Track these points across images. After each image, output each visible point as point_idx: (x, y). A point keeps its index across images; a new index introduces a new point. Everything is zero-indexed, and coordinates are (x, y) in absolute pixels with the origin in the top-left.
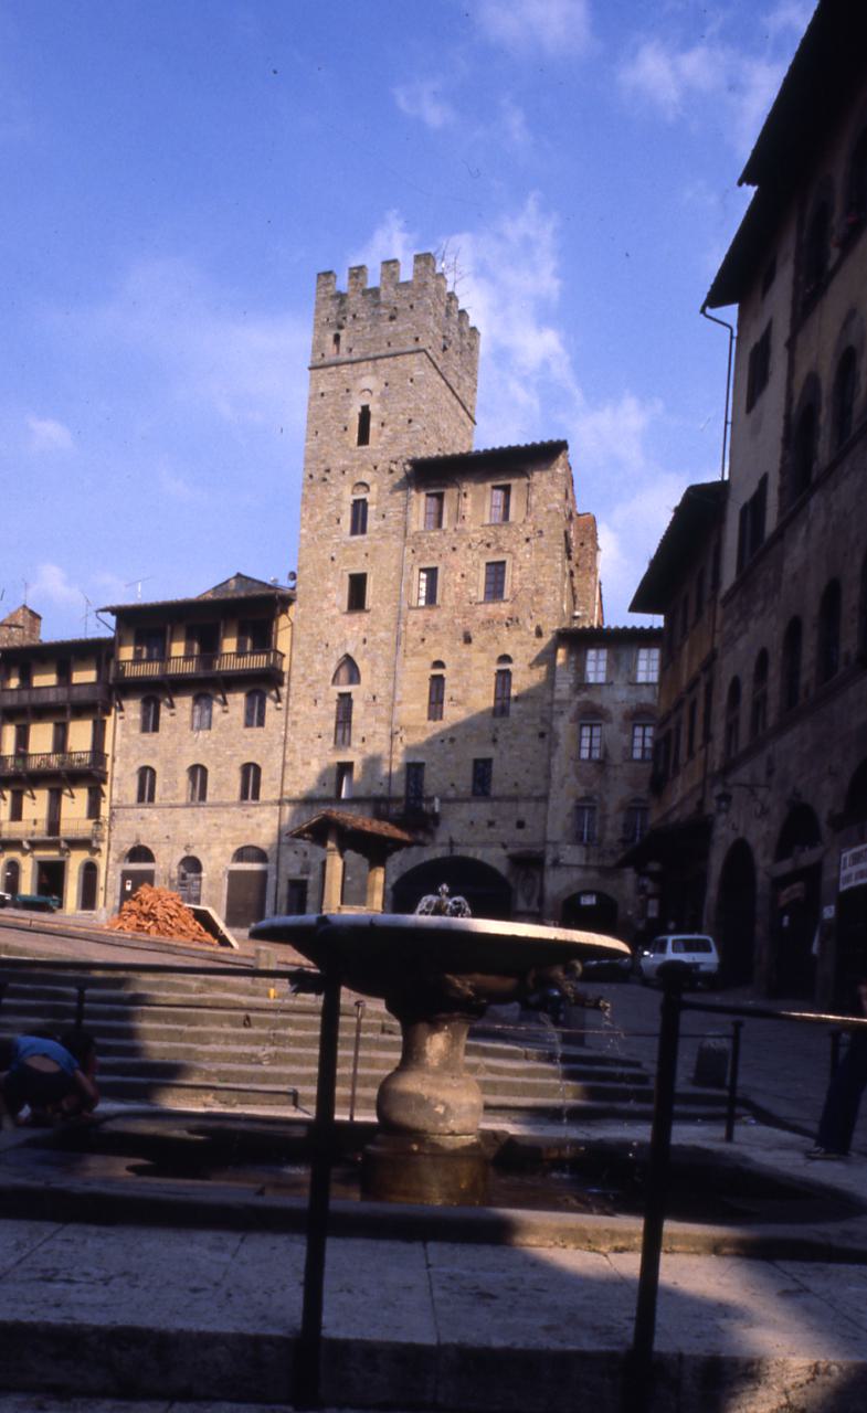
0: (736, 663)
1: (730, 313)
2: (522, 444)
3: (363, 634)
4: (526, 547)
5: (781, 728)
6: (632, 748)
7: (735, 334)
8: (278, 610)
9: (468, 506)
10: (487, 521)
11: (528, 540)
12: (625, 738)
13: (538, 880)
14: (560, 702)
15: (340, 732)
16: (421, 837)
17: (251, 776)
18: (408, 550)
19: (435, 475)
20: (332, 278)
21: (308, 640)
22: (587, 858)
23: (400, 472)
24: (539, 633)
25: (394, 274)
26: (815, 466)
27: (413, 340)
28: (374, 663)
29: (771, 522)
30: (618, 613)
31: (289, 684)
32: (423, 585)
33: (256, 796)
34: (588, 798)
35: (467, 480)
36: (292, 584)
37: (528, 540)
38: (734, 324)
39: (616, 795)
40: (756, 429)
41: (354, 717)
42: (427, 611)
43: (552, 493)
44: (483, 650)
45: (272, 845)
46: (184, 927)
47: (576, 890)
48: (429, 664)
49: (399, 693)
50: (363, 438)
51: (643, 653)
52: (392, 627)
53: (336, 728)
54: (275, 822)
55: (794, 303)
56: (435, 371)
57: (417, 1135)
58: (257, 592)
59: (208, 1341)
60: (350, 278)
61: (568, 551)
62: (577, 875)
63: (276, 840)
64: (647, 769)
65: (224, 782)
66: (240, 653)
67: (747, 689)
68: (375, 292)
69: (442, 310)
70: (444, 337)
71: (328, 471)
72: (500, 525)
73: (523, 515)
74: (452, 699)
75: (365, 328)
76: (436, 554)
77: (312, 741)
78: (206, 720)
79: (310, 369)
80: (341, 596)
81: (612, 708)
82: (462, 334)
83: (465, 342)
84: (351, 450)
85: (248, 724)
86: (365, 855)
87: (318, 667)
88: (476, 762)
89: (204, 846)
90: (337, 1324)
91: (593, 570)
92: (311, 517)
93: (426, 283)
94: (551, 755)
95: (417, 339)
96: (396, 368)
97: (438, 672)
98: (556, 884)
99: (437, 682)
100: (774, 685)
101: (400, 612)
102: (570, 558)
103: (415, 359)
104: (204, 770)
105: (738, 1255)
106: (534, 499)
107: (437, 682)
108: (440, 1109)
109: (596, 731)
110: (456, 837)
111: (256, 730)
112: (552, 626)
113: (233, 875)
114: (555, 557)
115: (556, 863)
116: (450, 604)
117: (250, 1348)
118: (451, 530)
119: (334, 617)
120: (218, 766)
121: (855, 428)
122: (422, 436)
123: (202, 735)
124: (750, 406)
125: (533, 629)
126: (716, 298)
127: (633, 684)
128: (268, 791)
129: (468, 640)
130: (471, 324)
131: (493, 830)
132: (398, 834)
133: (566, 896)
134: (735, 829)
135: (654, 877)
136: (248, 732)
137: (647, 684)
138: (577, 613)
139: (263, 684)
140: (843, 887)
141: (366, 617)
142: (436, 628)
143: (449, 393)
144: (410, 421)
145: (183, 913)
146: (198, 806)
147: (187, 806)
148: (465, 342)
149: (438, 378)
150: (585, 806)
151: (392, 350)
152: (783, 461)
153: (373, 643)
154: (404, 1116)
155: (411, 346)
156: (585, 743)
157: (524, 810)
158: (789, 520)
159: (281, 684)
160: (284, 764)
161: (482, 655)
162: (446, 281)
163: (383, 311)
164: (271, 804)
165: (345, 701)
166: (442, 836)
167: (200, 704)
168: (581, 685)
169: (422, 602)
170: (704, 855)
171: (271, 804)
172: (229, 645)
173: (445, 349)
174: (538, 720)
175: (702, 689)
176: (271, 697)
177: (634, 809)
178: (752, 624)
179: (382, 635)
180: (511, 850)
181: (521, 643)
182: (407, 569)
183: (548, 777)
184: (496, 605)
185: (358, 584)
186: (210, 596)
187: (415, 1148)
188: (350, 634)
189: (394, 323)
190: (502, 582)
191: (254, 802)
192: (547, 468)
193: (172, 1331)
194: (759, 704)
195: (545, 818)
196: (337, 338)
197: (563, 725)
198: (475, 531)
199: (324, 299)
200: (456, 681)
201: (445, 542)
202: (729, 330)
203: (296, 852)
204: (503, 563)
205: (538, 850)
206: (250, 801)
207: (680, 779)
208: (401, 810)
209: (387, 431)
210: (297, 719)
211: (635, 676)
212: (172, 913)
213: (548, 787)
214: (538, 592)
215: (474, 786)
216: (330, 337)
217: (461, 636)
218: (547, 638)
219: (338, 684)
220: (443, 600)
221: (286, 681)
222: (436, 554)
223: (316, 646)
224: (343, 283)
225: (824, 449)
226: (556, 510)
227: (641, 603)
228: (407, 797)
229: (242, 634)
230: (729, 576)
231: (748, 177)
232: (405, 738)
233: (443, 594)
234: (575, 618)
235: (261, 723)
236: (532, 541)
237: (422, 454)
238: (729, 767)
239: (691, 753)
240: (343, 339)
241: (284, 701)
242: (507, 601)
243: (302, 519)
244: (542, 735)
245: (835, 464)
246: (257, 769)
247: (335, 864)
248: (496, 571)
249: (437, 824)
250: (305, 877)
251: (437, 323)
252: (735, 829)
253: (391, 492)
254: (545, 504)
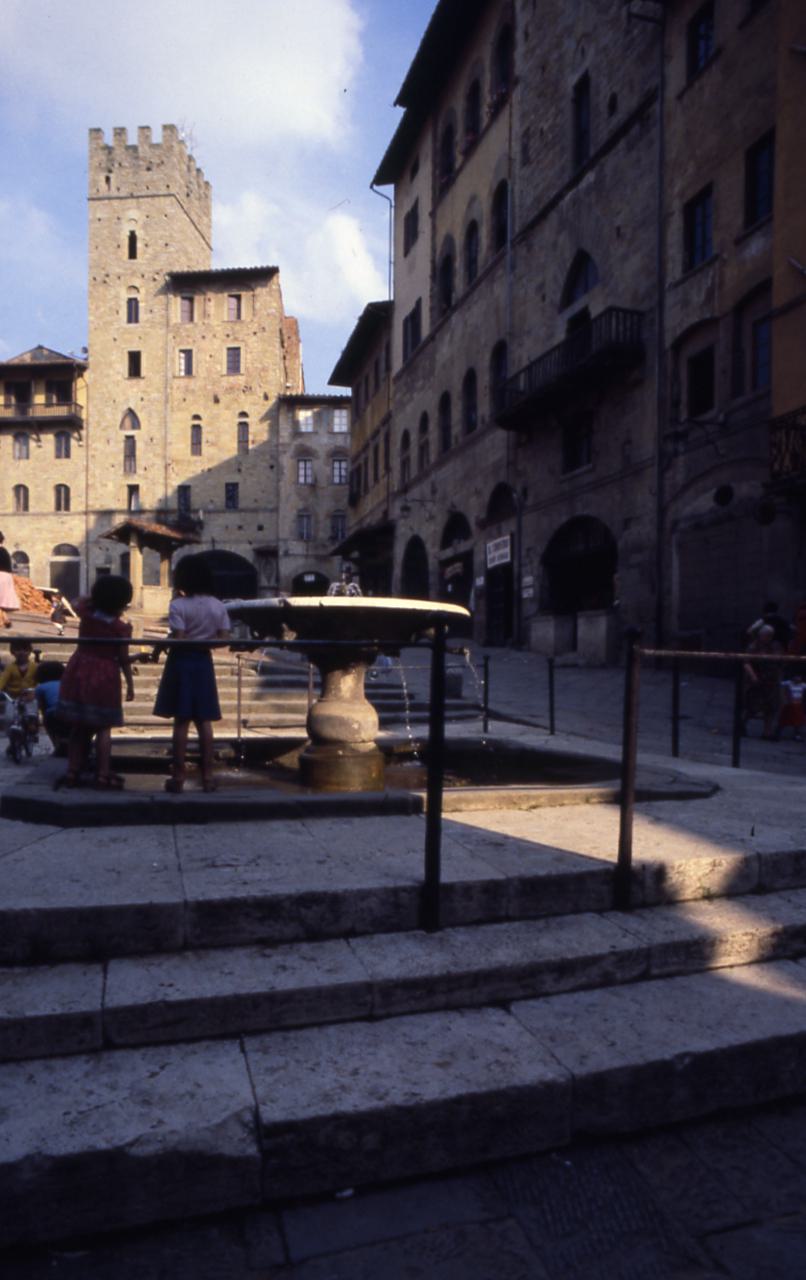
0: (405, 420)
1: (389, 189)
2: (248, 267)
3: (140, 395)
4: (254, 338)
5: (440, 463)
6: (333, 476)
7: (393, 204)
8: (76, 374)
9: (211, 307)
10: (226, 319)
11: (255, 333)
12: (328, 469)
13: (275, 565)
14: (283, 445)
15: (128, 463)
16: (191, 536)
17: (63, 496)
18: (170, 336)
19: (187, 284)
20: (101, 133)
21: (99, 395)
22: (307, 550)
23: (162, 280)
24: (266, 397)
25: (147, 137)
26: (454, 295)
27: (165, 187)
28: (150, 415)
29: (426, 329)
30: (319, 383)
31: (87, 429)
32: (183, 361)
33: (67, 508)
34: (305, 509)
35: (211, 291)
36: (85, 356)
37: (255, 333)
38: (392, 197)
39: (324, 507)
40: (411, 268)
41: (138, 453)
42: (186, 380)
43: (270, 302)
44: (228, 408)
45: (82, 544)
46: (37, 604)
47: (300, 571)
48: (190, 417)
49: (169, 436)
50: (133, 254)
51: (337, 413)
52: (162, 390)
53: (125, 461)
54: (83, 527)
55: (434, 188)
56: (182, 211)
57: (339, 743)
58: (60, 361)
59: (363, 895)
60: (115, 135)
61: (282, 343)
62: (301, 561)
63: (84, 540)
64: (345, 491)
65: (42, 498)
66: (48, 404)
67: (414, 437)
68: (135, 148)
69: (185, 168)
70: (187, 187)
71: (107, 276)
72: (235, 322)
73: (251, 316)
74: (207, 442)
75: (128, 173)
76: (190, 340)
77: (107, 469)
78: (24, 451)
79: (89, 199)
80: (124, 366)
81: (318, 449)
82: (199, 186)
83: (202, 192)
84: (124, 262)
85: (58, 456)
86: (158, 550)
87: (109, 417)
88: (227, 485)
89: (30, 544)
90: (447, 876)
91: (296, 355)
92: (97, 308)
93: (172, 146)
94: (279, 481)
95: (168, 186)
96: (153, 205)
97: (196, 422)
98: (287, 568)
99: (197, 429)
100: (434, 433)
101: (167, 380)
102: (283, 346)
103: (168, 200)
104: (26, 489)
105: (600, 803)
106: (258, 305)
107: (197, 429)
108: (356, 726)
109: (309, 464)
110: (215, 535)
111: (65, 461)
112: (274, 394)
113: (53, 565)
114: (275, 346)
115: (286, 554)
116: (202, 376)
117: (392, 896)
118: (200, 323)
119: (118, 381)
120: (37, 486)
121: (480, 273)
122: (175, 256)
123: (23, 463)
124: (407, 252)
125: (262, 395)
126: (381, 178)
127: (332, 433)
128: (76, 504)
129: (217, 401)
130: (205, 179)
131: (242, 532)
132: (173, 534)
133: (293, 576)
134: (411, 529)
135: (354, 561)
136: (58, 461)
137: (341, 433)
138: (288, 384)
139: (67, 428)
140: (490, 566)
141: (142, 382)
142: (193, 391)
143: (193, 228)
144: (167, 245)
145: (36, 593)
146: (23, 515)
147: (14, 515)
148: (202, 192)
149: (185, 216)
150: (304, 515)
151: (149, 193)
152: (431, 290)
153: (149, 400)
154: (330, 732)
155: (164, 191)
156: (302, 472)
157: (261, 518)
158: (438, 329)
159: (81, 427)
160: (87, 486)
161: (227, 412)
162: (186, 147)
163: (141, 163)
164: (79, 514)
165: (130, 441)
166: (206, 536)
167: (19, 442)
168: (297, 433)
169: (183, 374)
170: (390, 546)
171: (79, 514)
172: (40, 399)
173: (188, 195)
174: (268, 457)
175: (381, 437)
176: (75, 438)
177: (337, 517)
178: (415, 395)
179: (155, 395)
180: (255, 546)
181: (254, 404)
182: (170, 350)
183: (278, 495)
184: (236, 377)
185: (135, 359)
186: (28, 359)
187: (341, 753)
188: (131, 394)
189: (150, 172)
190: (239, 362)
191: (65, 512)
192: (265, 286)
193: (340, 891)
194: (424, 448)
195: (277, 523)
196: (108, 179)
197: (286, 461)
198: (218, 326)
199: (96, 149)
200: (209, 429)
201: (197, 332)
202: (388, 202)
203: (100, 548)
204: (238, 349)
205: (274, 544)
206: (63, 512)
207: (369, 497)
208: (176, 519)
209: (150, 250)
210: (96, 453)
211: (332, 429)
212: (28, 594)
213: (278, 502)
214: (264, 369)
215: (227, 503)
216: (102, 178)
217: (212, 399)
218: (272, 401)
219: (125, 429)
220: (197, 372)
221: (85, 425)
222: (190, 340)
223: (106, 402)
224: (109, 139)
225: (459, 283)
226: (273, 314)
227: (335, 380)
228: (179, 510)
229: (49, 391)
230: (397, 363)
231: (400, 101)
232: (176, 469)
233: (197, 366)
234: (288, 388)
235: (68, 455)
236: (258, 334)
237: (177, 269)
238: (405, 489)
239: (376, 479)
240: (112, 180)
241: (85, 440)
242: (242, 375)
243: (89, 309)
244: (272, 467)
245: (467, 295)
246: (67, 489)
247: (137, 559)
248: (234, 354)
249: (202, 528)
250: (108, 566)
251: (182, 177)
252: (411, 529)
253: (155, 296)
254: (265, 309)
